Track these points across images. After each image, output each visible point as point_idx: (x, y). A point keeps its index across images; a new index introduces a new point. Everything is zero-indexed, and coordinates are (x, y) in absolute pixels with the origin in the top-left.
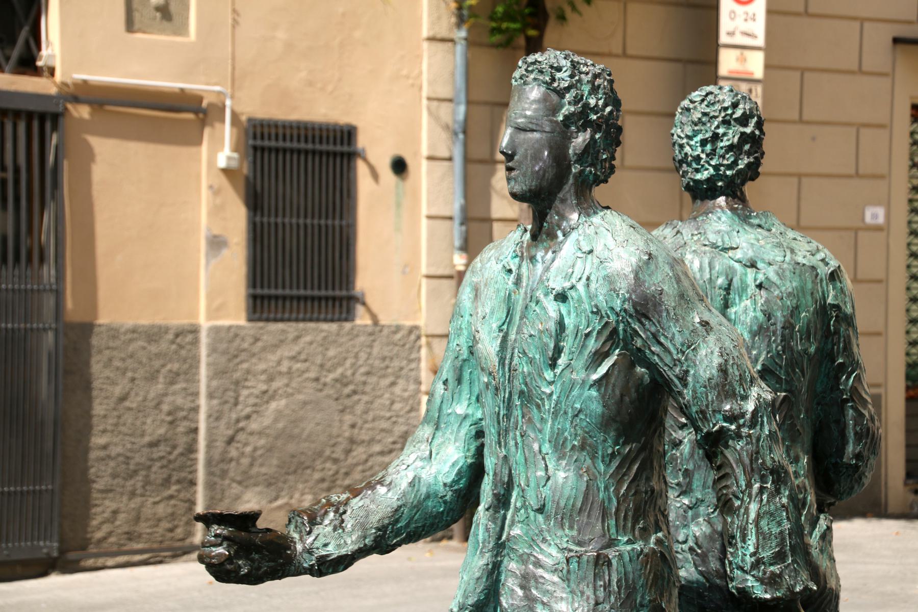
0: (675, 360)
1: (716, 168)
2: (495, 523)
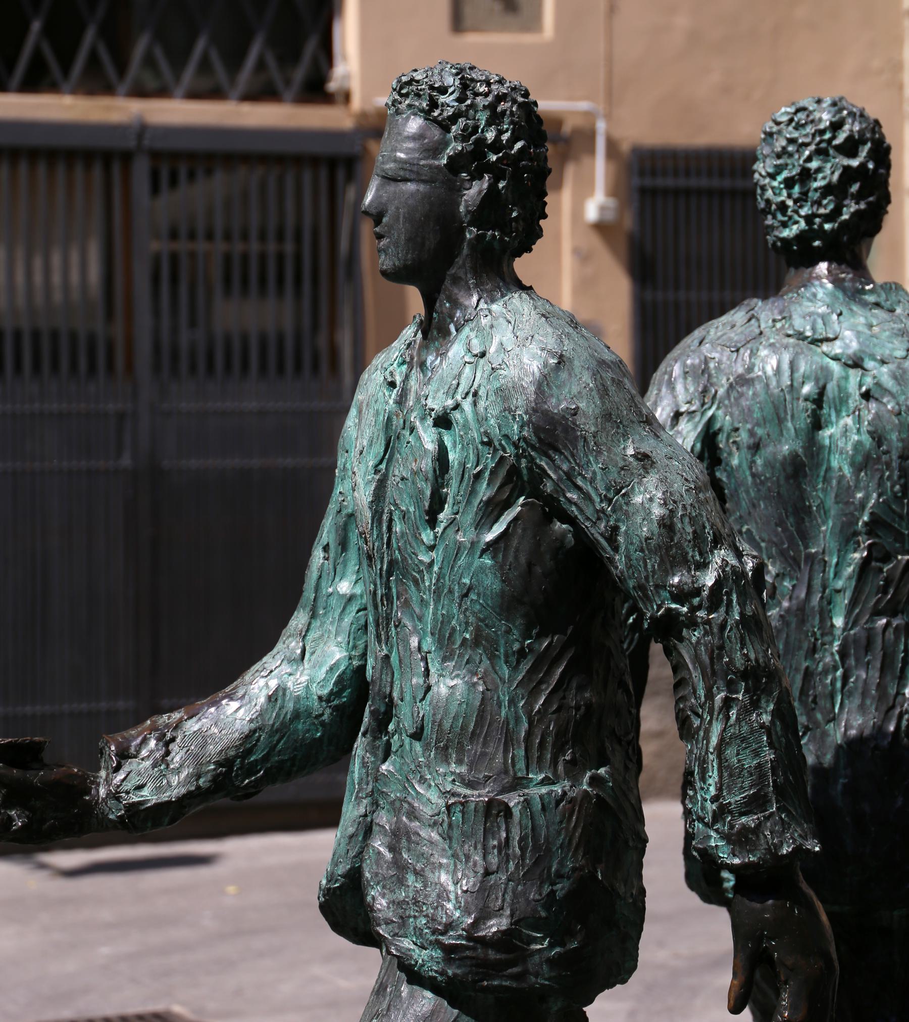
0: (597, 511)
1: (809, 219)
2: (374, 754)
